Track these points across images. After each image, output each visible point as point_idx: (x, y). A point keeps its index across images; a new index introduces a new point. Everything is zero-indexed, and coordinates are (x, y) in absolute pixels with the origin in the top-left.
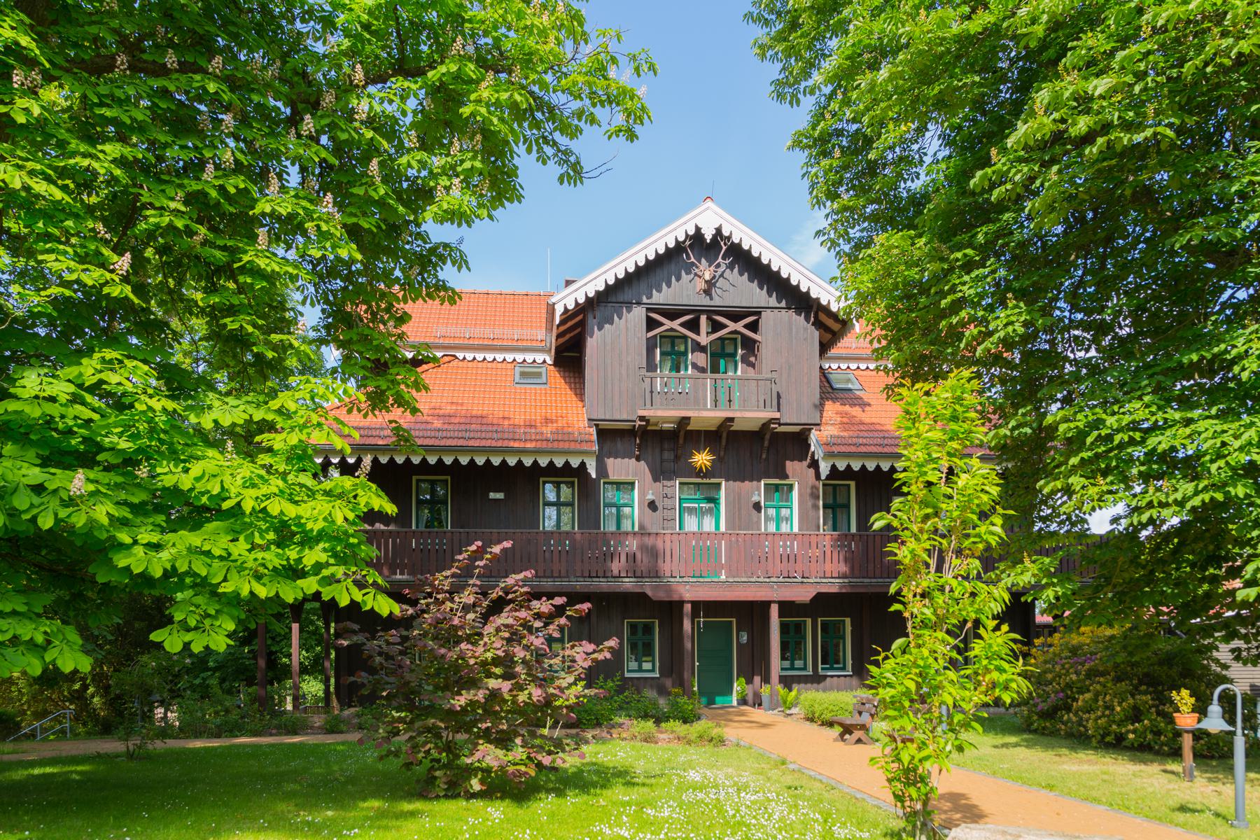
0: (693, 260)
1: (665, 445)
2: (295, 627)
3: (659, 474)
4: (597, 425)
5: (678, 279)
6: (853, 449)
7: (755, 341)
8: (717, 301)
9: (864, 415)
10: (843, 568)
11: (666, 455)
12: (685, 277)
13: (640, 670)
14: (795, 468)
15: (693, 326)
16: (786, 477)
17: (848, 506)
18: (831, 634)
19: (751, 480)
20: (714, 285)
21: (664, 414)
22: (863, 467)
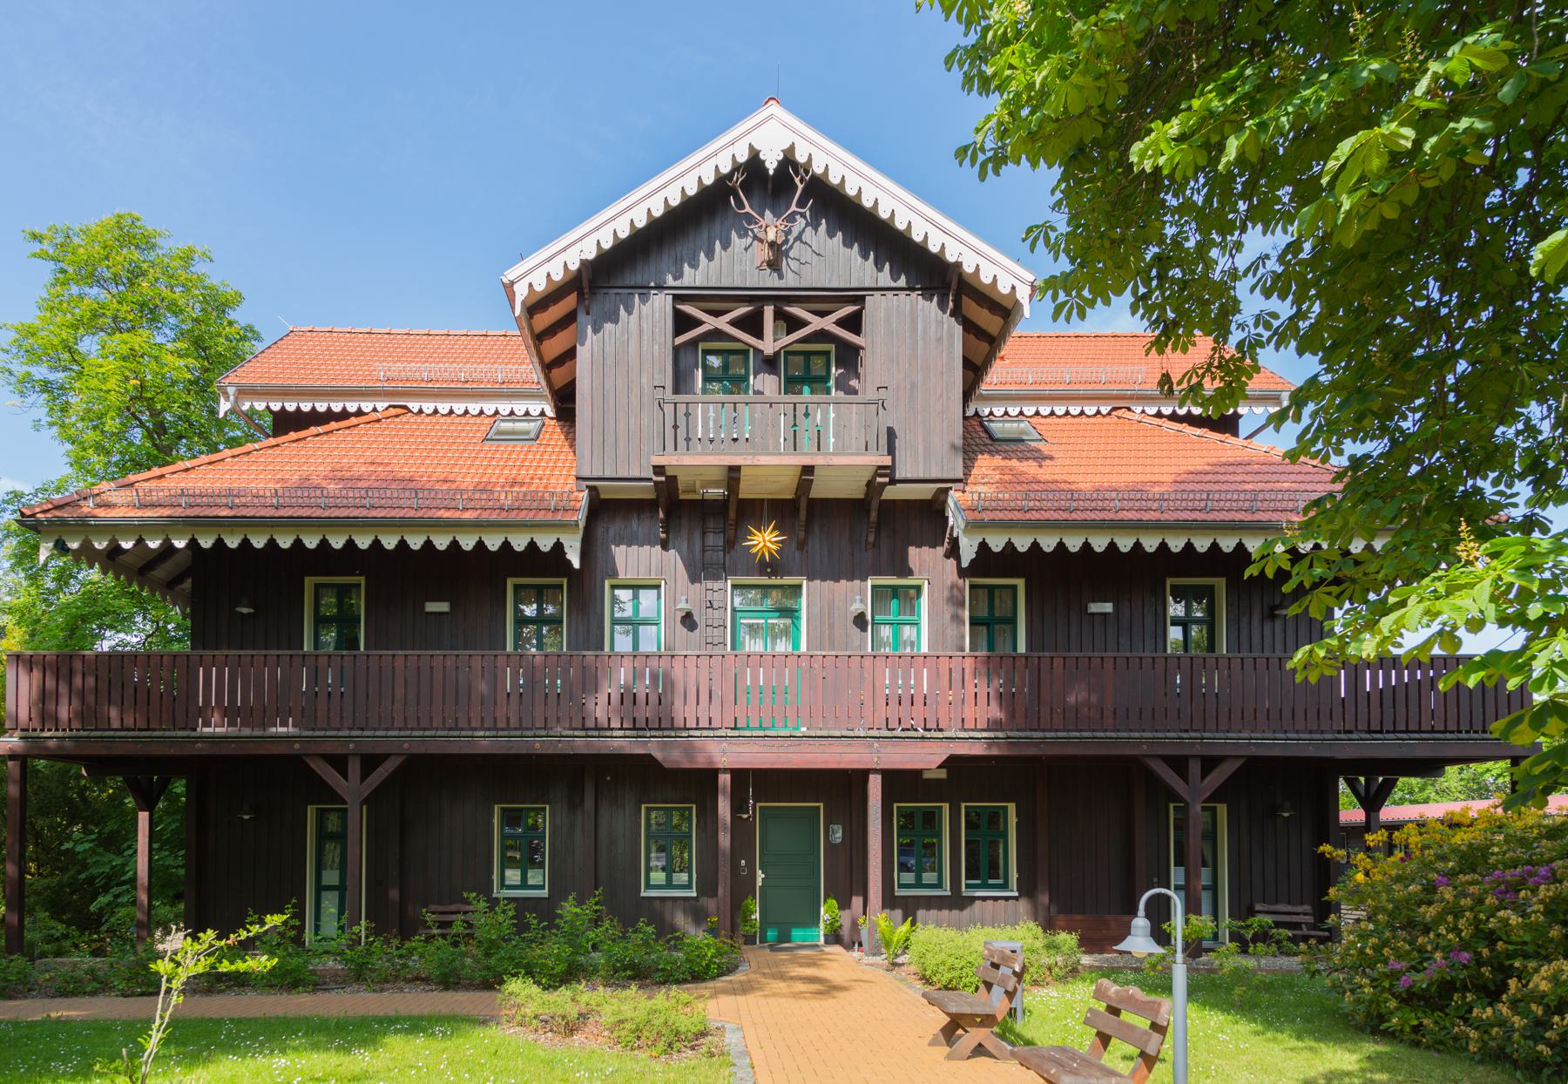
0: (748, 209)
1: (702, 518)
2: (143, 817)
3: (699, 570)
4: (592, 489)
5: (725, 247)
6: (1018, 516)
7: (856, 350)
8: (790, 280)
9: (1041, 471)
10: (995, 712)
11: (712, 539)
12: (738, 242)
13: (669, 885)
14: (929, 565)
15: (752, 324)
16: (908, 572)
17: (1012, 621)
18: (985, 829)
19: (851, 579)
20: (786, 254)
21: (698, 464)
22: (1035, 545)
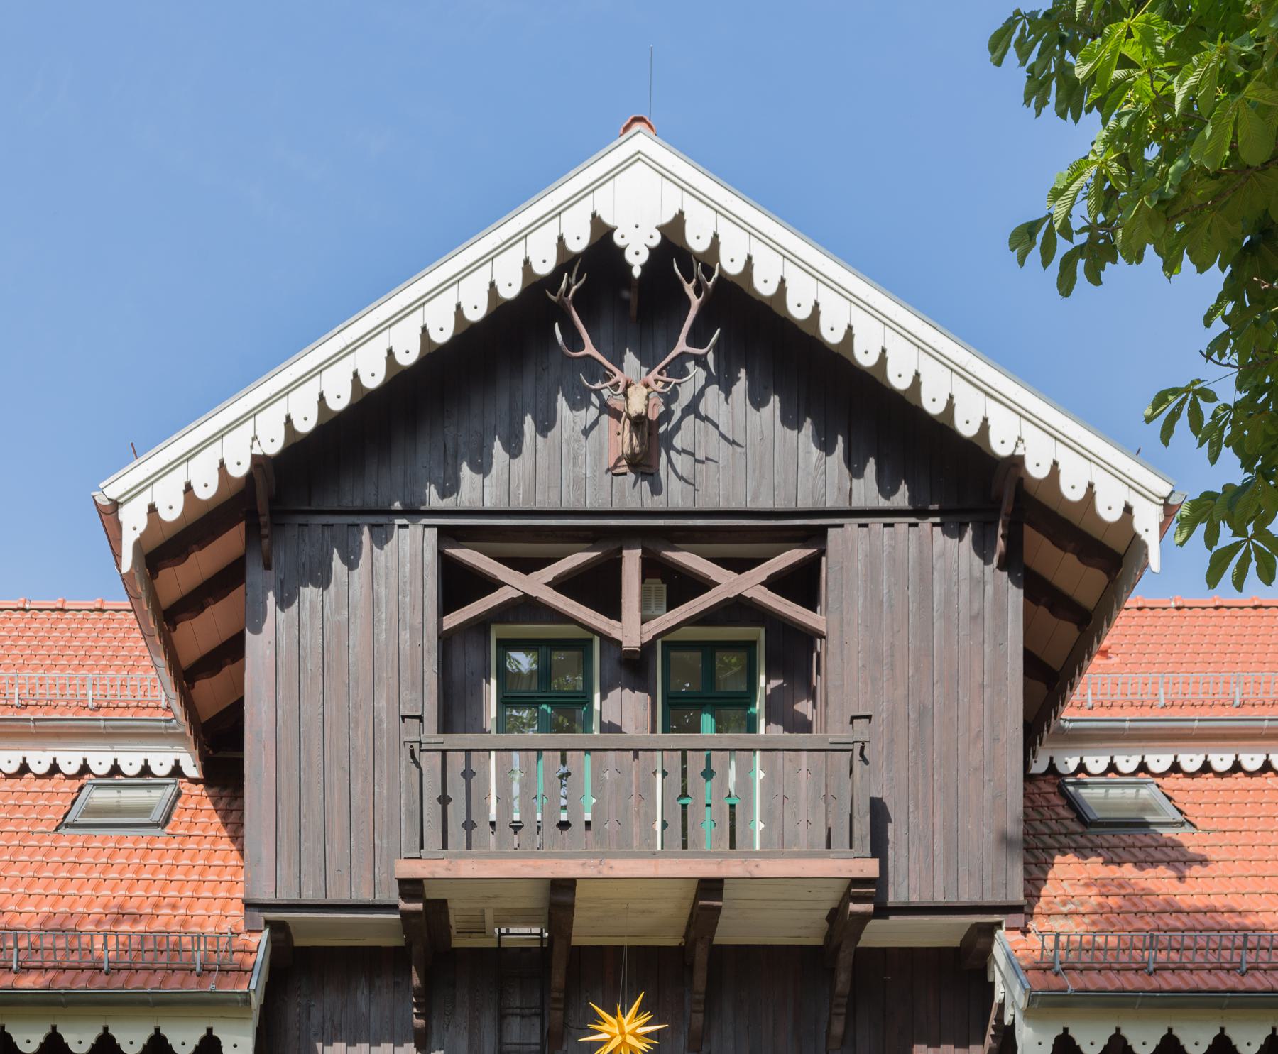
0: (589, 349)
5: (544, 428)
6: (1135, 981)
8: (675, 496)
9: (1182, 888)
12: (569, 419)
15: (598, 587)
21: (487, 869)
